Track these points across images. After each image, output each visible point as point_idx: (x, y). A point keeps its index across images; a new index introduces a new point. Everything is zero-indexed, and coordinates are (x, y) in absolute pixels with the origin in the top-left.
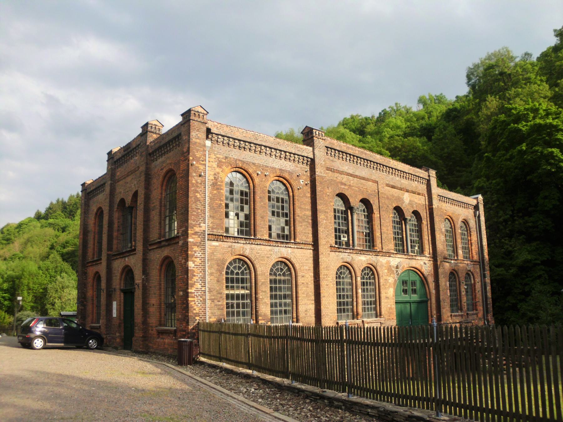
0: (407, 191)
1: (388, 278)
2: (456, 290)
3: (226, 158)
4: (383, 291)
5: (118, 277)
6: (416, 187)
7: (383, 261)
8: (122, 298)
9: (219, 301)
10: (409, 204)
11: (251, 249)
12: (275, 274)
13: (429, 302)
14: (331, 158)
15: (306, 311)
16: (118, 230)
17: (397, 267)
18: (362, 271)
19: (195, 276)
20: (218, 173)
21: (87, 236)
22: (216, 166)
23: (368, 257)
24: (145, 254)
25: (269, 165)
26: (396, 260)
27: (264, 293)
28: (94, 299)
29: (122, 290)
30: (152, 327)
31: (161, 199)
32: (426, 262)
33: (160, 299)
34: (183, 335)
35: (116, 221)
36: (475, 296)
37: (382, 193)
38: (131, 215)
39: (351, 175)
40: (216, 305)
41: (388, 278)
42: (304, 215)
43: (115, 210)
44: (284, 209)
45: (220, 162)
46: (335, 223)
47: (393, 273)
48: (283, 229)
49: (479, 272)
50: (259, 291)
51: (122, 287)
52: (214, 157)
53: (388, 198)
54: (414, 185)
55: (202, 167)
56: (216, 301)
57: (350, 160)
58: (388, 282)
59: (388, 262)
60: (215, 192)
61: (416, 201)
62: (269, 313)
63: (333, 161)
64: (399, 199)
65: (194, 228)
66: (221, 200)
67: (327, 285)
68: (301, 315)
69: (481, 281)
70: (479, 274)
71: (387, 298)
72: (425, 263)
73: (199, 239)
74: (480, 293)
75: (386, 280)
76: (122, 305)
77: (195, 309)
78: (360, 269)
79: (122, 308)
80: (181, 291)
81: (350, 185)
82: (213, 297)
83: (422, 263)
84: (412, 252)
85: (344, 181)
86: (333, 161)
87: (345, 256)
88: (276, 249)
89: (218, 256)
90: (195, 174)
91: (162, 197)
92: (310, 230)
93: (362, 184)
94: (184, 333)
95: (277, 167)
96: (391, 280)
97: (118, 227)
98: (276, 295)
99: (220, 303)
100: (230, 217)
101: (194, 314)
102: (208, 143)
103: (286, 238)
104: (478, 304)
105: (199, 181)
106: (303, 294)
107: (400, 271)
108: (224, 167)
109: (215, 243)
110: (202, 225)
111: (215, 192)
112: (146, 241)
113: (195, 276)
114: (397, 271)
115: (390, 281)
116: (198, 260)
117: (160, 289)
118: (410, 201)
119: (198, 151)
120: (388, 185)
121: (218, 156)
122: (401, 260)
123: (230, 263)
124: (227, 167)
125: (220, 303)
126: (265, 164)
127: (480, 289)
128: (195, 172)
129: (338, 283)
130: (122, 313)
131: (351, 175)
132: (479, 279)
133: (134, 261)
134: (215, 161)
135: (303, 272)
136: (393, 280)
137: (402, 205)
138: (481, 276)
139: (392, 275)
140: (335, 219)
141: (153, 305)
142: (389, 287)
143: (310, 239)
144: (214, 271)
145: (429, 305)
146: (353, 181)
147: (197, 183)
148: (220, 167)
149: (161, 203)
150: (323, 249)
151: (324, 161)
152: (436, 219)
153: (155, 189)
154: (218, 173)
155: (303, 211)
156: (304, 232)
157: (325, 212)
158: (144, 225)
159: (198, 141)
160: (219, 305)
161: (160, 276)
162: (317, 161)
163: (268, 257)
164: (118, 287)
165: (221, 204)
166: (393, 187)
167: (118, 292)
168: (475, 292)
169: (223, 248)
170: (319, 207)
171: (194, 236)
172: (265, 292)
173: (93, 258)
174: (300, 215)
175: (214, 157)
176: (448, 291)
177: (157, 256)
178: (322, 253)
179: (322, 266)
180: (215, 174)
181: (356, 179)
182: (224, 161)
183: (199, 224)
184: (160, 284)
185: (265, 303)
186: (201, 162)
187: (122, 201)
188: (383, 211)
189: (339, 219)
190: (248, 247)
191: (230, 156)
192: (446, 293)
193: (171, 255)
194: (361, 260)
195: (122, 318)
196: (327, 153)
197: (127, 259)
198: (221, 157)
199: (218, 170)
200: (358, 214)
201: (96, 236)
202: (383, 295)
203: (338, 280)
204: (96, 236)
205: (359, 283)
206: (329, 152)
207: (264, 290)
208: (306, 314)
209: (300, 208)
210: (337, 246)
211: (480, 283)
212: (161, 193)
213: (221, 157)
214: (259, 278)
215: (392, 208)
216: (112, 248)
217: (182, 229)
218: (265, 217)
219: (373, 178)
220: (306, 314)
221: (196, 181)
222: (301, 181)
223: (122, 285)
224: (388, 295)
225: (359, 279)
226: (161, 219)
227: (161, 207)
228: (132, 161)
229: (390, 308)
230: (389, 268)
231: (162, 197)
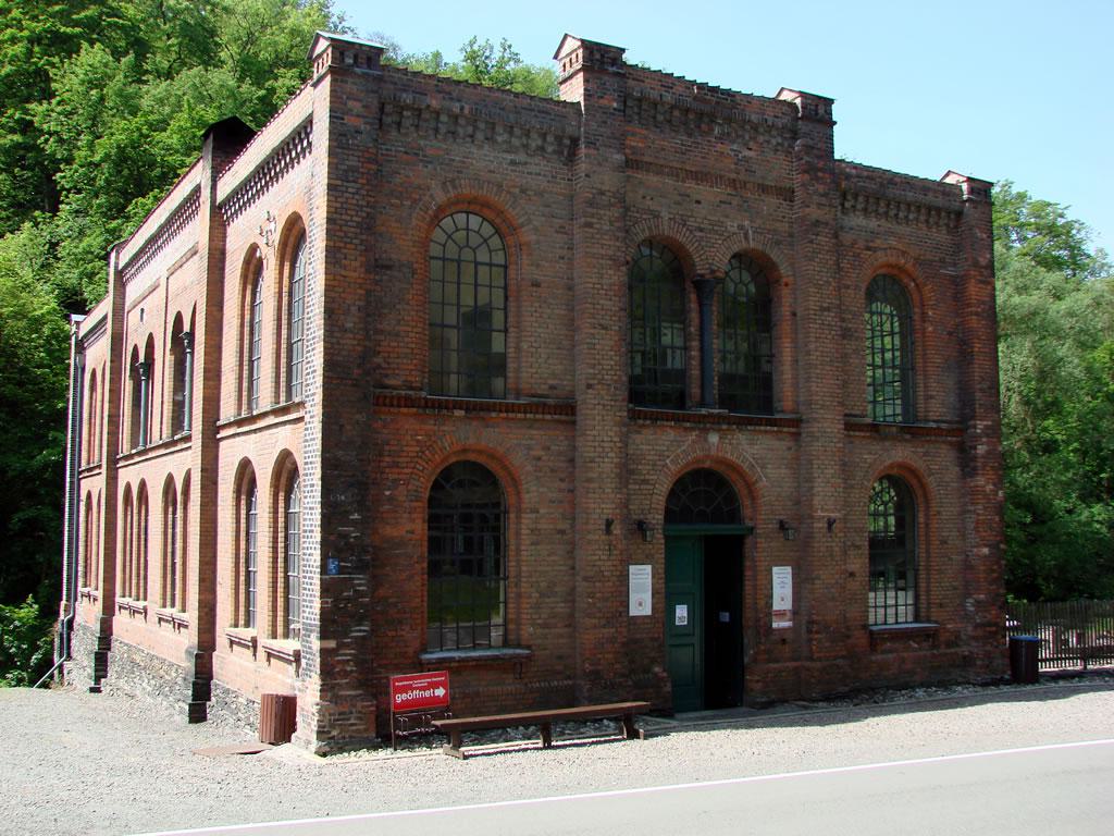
80: (986, 546)
94: (994, 629)
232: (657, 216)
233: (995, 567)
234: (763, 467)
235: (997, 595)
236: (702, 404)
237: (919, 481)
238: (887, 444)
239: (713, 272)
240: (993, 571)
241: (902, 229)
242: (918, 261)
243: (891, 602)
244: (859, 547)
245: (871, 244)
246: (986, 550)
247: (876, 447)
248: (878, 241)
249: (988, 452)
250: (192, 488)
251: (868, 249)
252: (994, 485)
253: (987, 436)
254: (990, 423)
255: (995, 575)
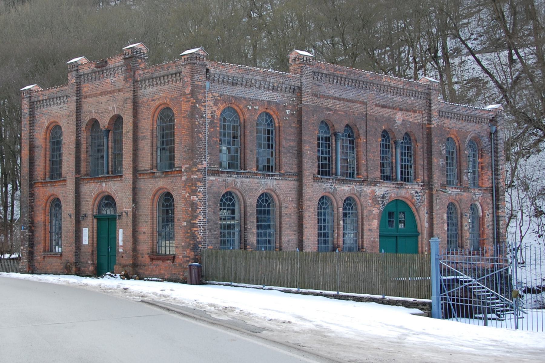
0: (401, 110)
1: (372, 209)
2: (455, 224)
3: (221, 95)
4: (365, 223)
5: (91, 203)
6: (412, 103)
7: (367, 191)
8: (95, 225)
9: (215, 231)
10: (402, 124)
11: (242, 182)
12: (261, 206)
13: (420, 237)
14: (318, 83)
15: (288, 241)
16: (87, 152)
17: (383, 197)
18: (345, 201)
19: (198, 208)
20: (215, 111)
21: (34, 152)
22: (212, 105)
23: (352, 186)
24: (135, 182)
25: (258, 98)
26: (383, 189)
27: (252, 224)
28: (47, 223)
29: (95, 217)
30: (143, 254)
31: (152, 130)
32: (419, 191)
33: (153, 228)
34: (187, 260)
35: (83, 142)
36: (483, 231)
37: (370, 115)
38: (108, 138)
39: (337, 99)
40: (212, 234)
41: (372, 209)
42: (289, 146)
43: (83, 129)
44: (270, 138)
45: (216, 100)
46: (319, 151)
47: (379, 204)
48: (269, 161)
49: (491, 203)
50: (248, 222)
51: (95, 213)
52: (211, 96)
53: (377, 120)
54: (409, 102)
55: (203, 109)
56: (212, 231)
57: (337, 82)
58: (372, 213)
59: (373, 192)
60: (212, 130)
61: (411, 120)
62: (255, 242)
63: (319, 86)
64: (391, 120)
65: (198, 165)
66: (217, 137)
67: (309, 216)
68: (284, 245)
69: (493, 214)
70: (490, 206)
71: (370, 230)
72: (417, 192)
73: (201, 175)
74: (491, 228)
75: (370, 211)
76: (95, 232)
77: (198, 238)
78: (342, 200)
79: (95, 235)
80: (185, 221)
81: (336, 110)
82: (210, 227)
83: (413, 192)
84: (402, 180)
85: (330, 105)
86: (319, 86)
87: (327, 186)
88: (263, 181)
89: (215, 189)
90: (197, 116)
91: (153, 128)
92: (295, 161)
93: (348, 107)
94: (188, 259)
95: (265, 99)
96: (376, 211)
97: (87, 148)
98: (261, 225)
99: (216, 233)
100: (223, 152)
101: (197, 242)
102: (207, 84)
103: (269, 169)
104: (486, 241)
105: (201, 122)
106: (286, 224)
107: (386, 202)
108: (219, 105)
109: (212, 178)
110: (203, 162)
111: (212, 130)
112: (136, 171)
113: (198, 208)
114: (383, 201)
115: (374, 212)
116: (200, 194)
117: (153, 217)
118: (403, 120)
119: (200, 93)
120: (377, 105)
121: (214, 94)
122: (388, 189)
123: (223, 196)
124: (222, 104)
125: (216, 233)
126: (254, 98)
127: (491, 223)
128: (198, 114)
129: (319, 214)
130: (95, 240)
131: (337, 99)
132: (491, 211)
133: (120, 190)
134: (212, 100)
135: (287, 204)
136: (378, 211)
137: (393, 126)
138: (493, 208)
139: (376, 206)
140: (319, 147)
141: (144, 233)
142: (373, 218)
143: (295, 170)
144: (211, 204)
145: (420, 240)
146: (339, 105)
147: (200, 124)
148: (217, 106)
149: (152, 133)
150: (307, 179)
151: (311, 88)
152: (435, 140)
153: (145, 119)
154: (215, 111)
155: (288, 142)
156: (288, 162)
157: (310, 142)
158: (133, 154)
159: (199, 83)
160: (215, 234)
161: (152, 205)
162: (303, 89)
163: (256, 190)
164: (90, 213)
165: (217, 141)
166: (384, 107)
167: (90, 218)
168: (483, 227)
169: (219, 182)
170: (304, 138)
171: (197, 173)
172: (253, 222)
173: (45, 178)
174: (285, 146)
175: (211, 96)
176: (446, 225)
177: (151, 187)
178: (306, 185)
179: (306, 197)
180: (212, 113)
181: (342, 102)
182: (219, 98)
183: (202, 162)
184: (153, 213)
185: (253, 232)
186: (203, 104)
187: (94, 123)
188: (371, 135)
189: (326, 158)
190: (239, 180)
191: (225, 93)
192: (442, 227)
193: (170, 189)
194: (344, 190)
195: (95, 245)
196: (314, 78)
197: (104, 185)
198: (217, 95)
199: (215, 108)
200: (343, 139)
201: (48, 153)
202: (366, 227)
203: (319, 211)
204: (48, 153)
205: (341, 214)
206: (315, 77)
207: (251, 220)
208: (288, 245)
209: (286, 139)
210: (319, 176)
211: (490, 217)
212: (153, 124)
213: (217, 95)
214: (248, 209)
215: (380, 131)
216: (80, 171)
217: (185, 166)
218: (255, 153)
219: (362, 99)
220: (288, 245)
221: (198, 122)
222: (287, 111)
223: (95, 210)
224: (371, 228)
225: (341, 210)
226: (153, 150)
227: (153, 138)
228: (108, 80)
229: (374, 242)
230: (374, 199)
231: (153, 128)
232: (91, 112)
233: (189, 231)
234: (117, 193)
235: (190, 244)
236: (103, 173)
237: (100, 193)
238: (157, 179)
239: (104, 127)
240: (188, 233)
241: (166, 87)
242: (171, 99)
243: (167, 249)
244: (147, 222)
245: (154, 98)
246: (185, 224)
247: (153, 181)
248: (156, 96)
249: (187, 179)
250: (37, 163)
251: (153, 100)
252: (189, 193)
253: (187, 172)
254: (188, 166)
255: (189, 235)
